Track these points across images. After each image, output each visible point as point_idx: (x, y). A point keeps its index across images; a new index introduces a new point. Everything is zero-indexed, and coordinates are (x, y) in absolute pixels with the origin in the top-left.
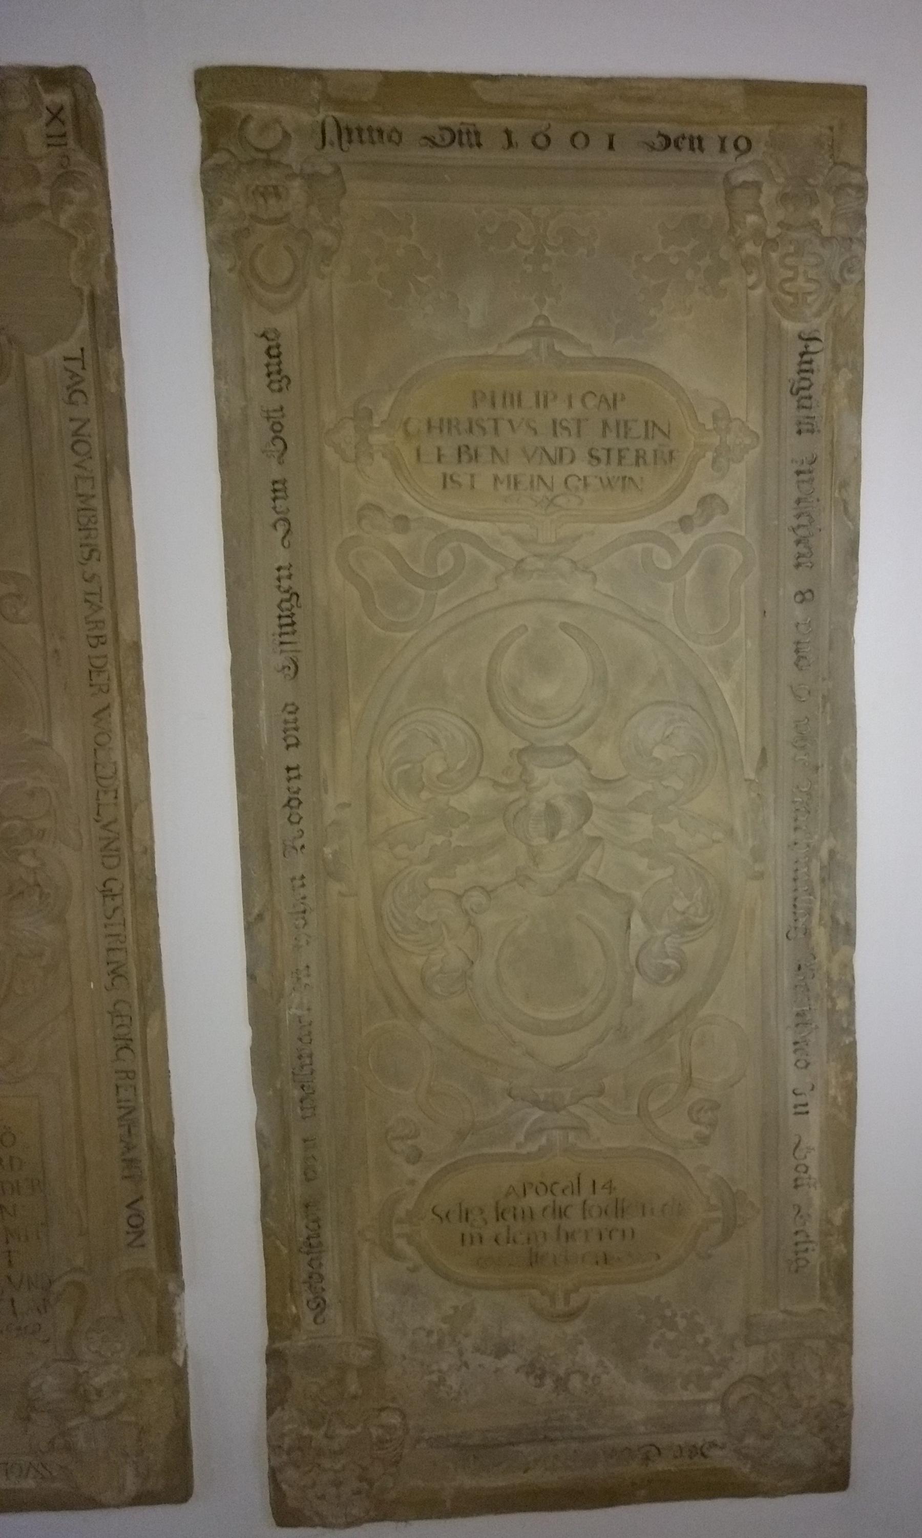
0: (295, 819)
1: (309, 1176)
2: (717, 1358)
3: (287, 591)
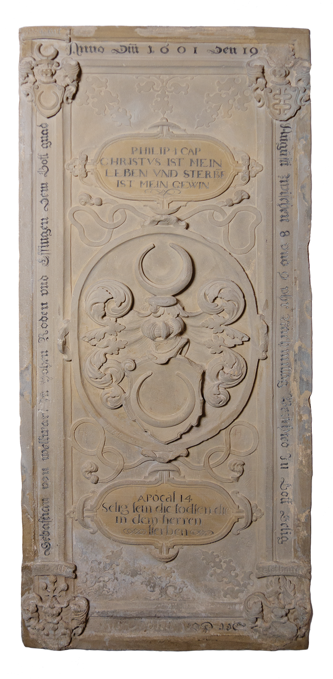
0: (44, 326)
1: (45, 486)
2: (242, 583)
3: (45, 229)
